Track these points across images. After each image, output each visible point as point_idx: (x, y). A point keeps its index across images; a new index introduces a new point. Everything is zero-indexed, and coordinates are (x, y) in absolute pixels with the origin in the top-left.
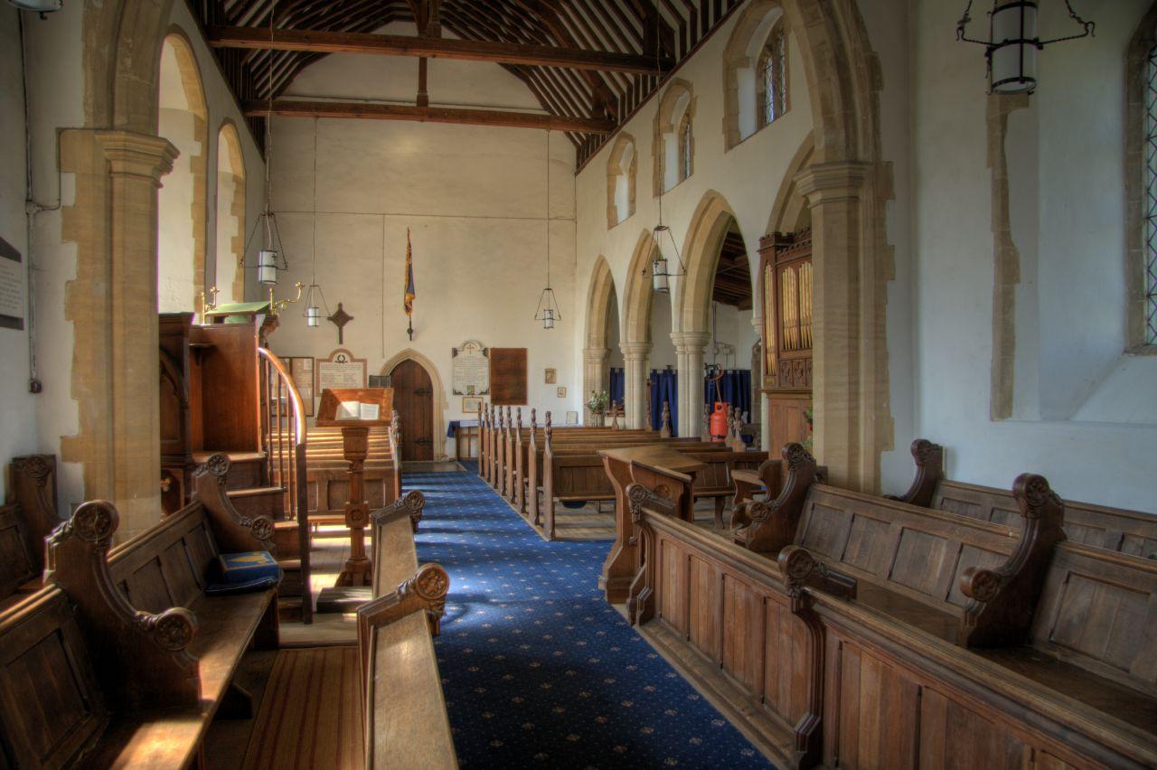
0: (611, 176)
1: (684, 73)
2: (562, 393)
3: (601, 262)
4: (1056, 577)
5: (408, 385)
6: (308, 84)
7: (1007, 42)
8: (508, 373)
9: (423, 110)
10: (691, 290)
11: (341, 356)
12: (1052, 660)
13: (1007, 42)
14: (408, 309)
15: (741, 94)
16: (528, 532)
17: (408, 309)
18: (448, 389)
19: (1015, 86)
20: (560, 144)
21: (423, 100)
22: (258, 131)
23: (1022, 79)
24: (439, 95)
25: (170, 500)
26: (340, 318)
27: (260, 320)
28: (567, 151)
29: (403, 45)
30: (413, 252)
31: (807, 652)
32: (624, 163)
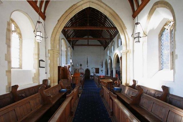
0: (107, 51)
1: (113, 40)
2: (103, 72)
3: (106, 59)
4: (142, 97)
5: (88, 71)
6: (77, 43)
7: (137, 37)
8: (97, 71)
9: (88, 45)
10: (114, 62)
11: (81, 69)
12: (141, 107)
13: (137, 37)
14: (87, 64)
15: (119, 42)
16: (96, 87)
17: (87, 64)
18: (91, 72)
19: (138, 42)
20: (103, 48)
21: (88, 44)
22: (73, 47)
23: (139, 41)
24: (90, 43)
25: (58, 83)
26: (81, 65)
27: (68, 67)
28: (103, 48)
29: (85, 39)
30: (134, 49)
31: (54, 116)
32: (108, 49)
